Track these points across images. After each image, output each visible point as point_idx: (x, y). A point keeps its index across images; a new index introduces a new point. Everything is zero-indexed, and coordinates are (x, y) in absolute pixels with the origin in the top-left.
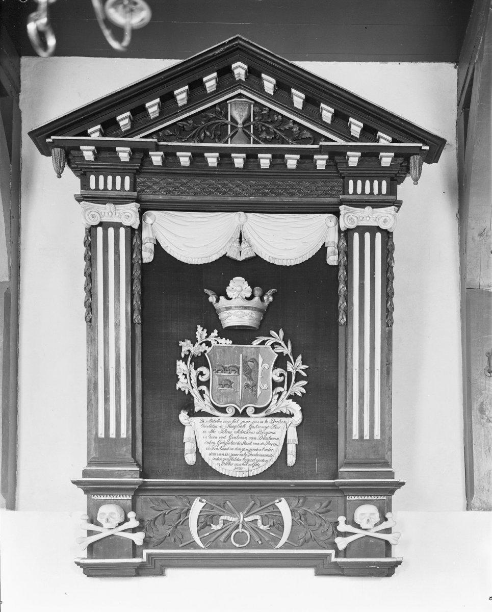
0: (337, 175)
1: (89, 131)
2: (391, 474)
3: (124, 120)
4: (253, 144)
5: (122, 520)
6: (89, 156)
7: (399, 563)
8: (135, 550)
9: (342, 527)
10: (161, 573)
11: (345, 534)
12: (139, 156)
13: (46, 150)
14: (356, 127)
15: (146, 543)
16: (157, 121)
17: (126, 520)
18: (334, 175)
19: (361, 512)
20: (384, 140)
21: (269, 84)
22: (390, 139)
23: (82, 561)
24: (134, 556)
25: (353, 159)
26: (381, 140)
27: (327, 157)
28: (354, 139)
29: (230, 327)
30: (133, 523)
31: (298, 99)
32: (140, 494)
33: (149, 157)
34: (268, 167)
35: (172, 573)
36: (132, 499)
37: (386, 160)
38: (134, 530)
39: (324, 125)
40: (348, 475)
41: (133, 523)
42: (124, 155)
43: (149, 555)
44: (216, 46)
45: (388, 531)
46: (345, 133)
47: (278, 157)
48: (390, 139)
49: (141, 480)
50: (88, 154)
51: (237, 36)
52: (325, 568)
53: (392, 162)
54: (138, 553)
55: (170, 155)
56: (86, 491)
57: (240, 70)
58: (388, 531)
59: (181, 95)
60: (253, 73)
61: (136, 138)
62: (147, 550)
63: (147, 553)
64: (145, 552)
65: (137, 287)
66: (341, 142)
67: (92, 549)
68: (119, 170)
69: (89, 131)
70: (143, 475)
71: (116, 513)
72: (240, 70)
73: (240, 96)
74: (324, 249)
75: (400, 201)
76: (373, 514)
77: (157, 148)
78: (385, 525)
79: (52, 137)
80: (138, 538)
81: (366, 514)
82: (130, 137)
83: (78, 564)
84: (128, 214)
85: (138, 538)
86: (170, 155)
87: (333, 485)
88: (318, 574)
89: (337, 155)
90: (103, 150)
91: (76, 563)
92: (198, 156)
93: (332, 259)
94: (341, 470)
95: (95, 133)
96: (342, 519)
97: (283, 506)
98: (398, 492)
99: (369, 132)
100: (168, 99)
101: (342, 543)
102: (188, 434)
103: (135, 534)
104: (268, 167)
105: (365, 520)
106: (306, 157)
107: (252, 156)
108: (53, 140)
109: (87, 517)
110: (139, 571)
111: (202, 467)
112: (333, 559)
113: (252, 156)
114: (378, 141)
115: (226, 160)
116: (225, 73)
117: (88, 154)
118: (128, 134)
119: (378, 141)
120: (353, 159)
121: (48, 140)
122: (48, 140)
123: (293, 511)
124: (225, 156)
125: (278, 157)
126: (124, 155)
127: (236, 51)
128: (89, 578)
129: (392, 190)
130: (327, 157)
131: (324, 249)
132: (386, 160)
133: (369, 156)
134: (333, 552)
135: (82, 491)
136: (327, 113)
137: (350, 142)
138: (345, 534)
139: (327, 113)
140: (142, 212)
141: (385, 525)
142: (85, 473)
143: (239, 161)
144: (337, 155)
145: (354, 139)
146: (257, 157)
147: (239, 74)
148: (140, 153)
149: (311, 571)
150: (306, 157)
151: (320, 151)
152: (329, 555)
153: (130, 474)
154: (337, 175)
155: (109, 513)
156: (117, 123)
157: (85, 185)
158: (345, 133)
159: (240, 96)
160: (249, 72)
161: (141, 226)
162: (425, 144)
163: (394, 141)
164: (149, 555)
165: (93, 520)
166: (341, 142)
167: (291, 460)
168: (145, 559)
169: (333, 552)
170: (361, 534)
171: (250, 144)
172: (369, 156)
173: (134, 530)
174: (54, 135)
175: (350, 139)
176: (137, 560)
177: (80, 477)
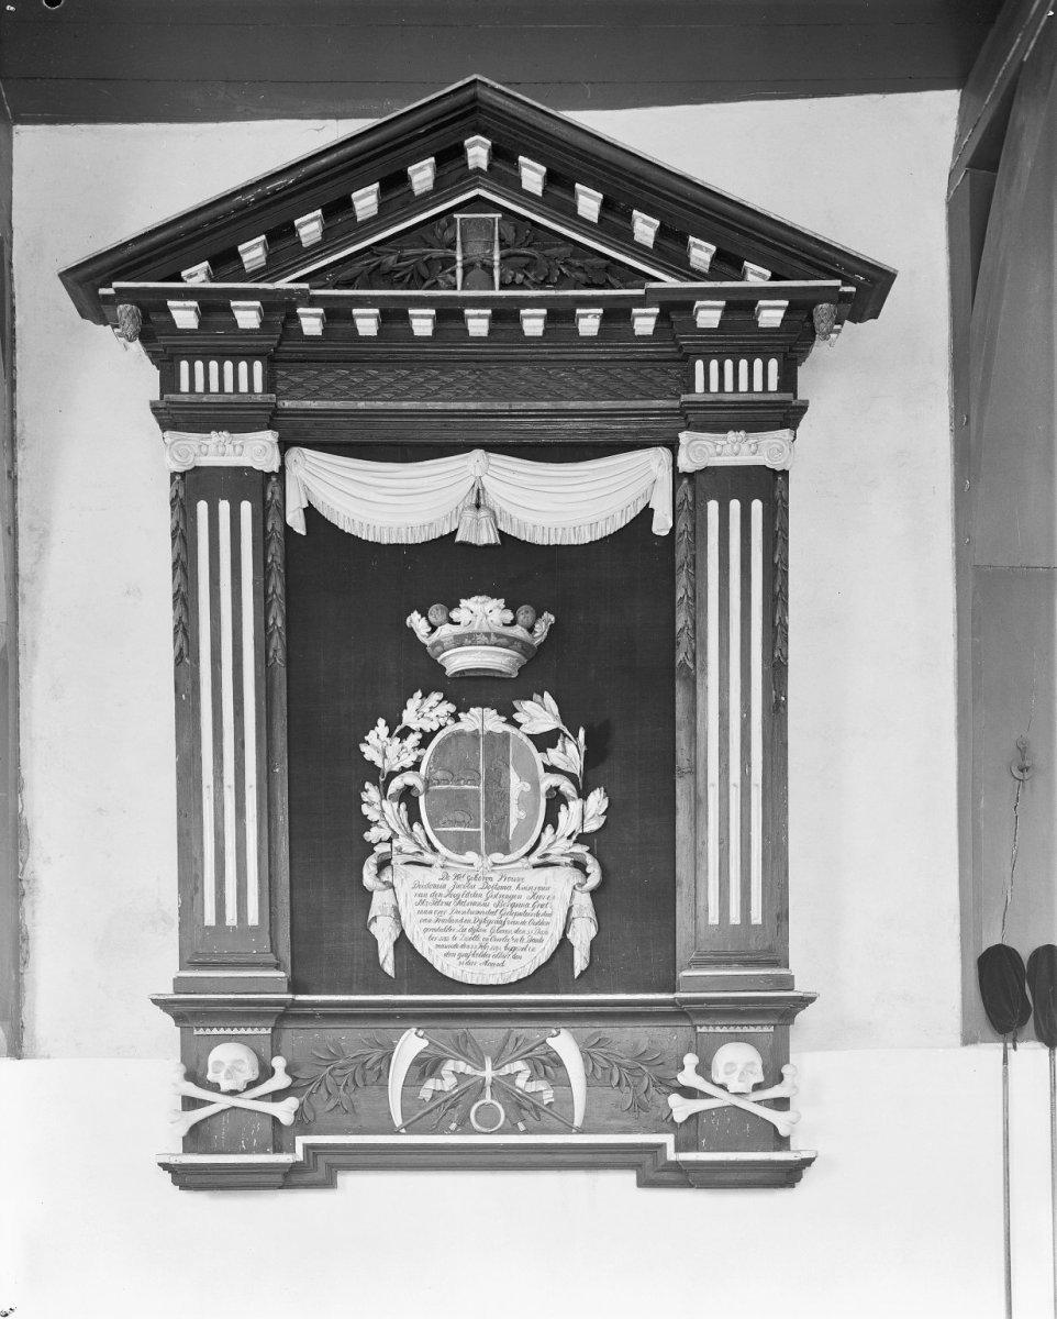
0: (674, 349)
1: (184, 274)
2: (787, 982)
3: (253, 253)
4: (501, 289)
5: (252, 1075)
6: (311, 326)
7: (808, 1162)
8: (278, 1137)
9: (688, 1077)
10: (329, 1183)
11: (689, 1093)
12: (279, 318)
13: (95, 308)
14: (701, 254)
15: (303, 1123)
16: (319, 249)
17: (267, 1072)
18: (670, 350)
19: (724, 1062)
20: (756, 276)
21: (532, 176)
22: (768, 274)
23: (172, 1161)
24: (278, 1149)
25: (709, 316)
26: (750, 277)
27: (657, 310)
28: (697, 275)
29: (463, 672)
30: (280, 1081)
31: (589, 203)
32: (285, 1026)
33: (296, 317)
34: (541, 334)
35: (352, 1183)
36: (272, 1035)
37: (771, 316)
38: (277, 1096)
39: (638, 250)
40: (696, 980)
41: (280, 1081)
42: (247, 317)
43: (307, 1147)
44: (433, 97)
45: (782, 1104)
46: (682, 268)
47: (561, 316)
48: (768, 274)
49: (290, 996)
50: (185, 316)
51: (475, 76)
52: (656, 1173)
53: (722, 317)
54: (285, 1143)
55: (337, 315)
56: (179, 1019)
57: (478, 152)
58: (782, 1104)
59: (366, 201)
60: (503, 155)
61: (282, 284)
62: (304, 1137)
63: (304, 1145)
64: (301, 1141)
65: (277, 585)
66: (670, 282)
67: (196, 1138)
68: (237, 348)
69: (184, 274)
70: (295, 986)
71: (246, 1061)
72: (478, 152)
73: (478, 203)
74: (647, 514)
75: (803, 401)
76: (753, 1063)
77: (313, 302)
78: (776, 1092)
79: (116, 284)
80: (285, 1111)
81: (737, 1063)
82: (270, 282)
83: (165, 1166)
84: (256, 450)
85: (285, 1111)
86: (337, 315)
87: (672, 1003)
88: (643, 1183)
89: (675, 310)
90: (213, 307)
91: (160, 1164)
92: (394, 316)
93: (661, 525)
94: (685, 973)
95: (197, 276)
96: (691, 1060)
97: (564, 1044)
98: (803, 1016)
99: (728, 262)
100: (337, 209)
101: (681, 1108)
102: (381, 902)
103: (275, 1104)
104: (541, 334)
105: (736, 1075)
106: (617, 315)
107: (505, 316)
108: (116, 289)
109: (182, 1069)
110: (288, 1178)
111: (415, 968)
112: (671, 1155)
113: (505, 316)
114: (742, 278)
115: (340, 326)
116: (450, 158)
117: (185, 316)
118: (257, 275)
119: (742, 278)
120: (709, 316)
121: (103, 291)
122: (103, 291)
123: (587, 1056)
124: (450, 315)
125: (561, 316)
126: (247, 317)
127: (469, 113)
128: (184, 1193)
129: (788, 381)
130: (656, 310)
131: (647, 514)
132: (771, 316)
133: (741, 306)
134: (668, 1139)
135: (169, 1020)
136: (645, 228)
137: (699, 281)
138: (689, 1093)
139: (645, 228)
140: (284, 446)
141: (776, 1092)
142: (179, 984)
143: (478, 325)
144: (675, 310)
145: (697, 275)
146: (685, 243)
147: (476, 156)
148: (279, 310)
149: (630, 1177)
150: (617, 315)
151: (641, 302)
152: (661, 1146)
153: (271, 983)
154: (674, 349)
155: (230, 1061)
156: (237, 257)
157: (169, 382)
158: (682, 268)
159: (478, 203)
160: (495, 153)
161: (283, 468)
162: (846, 282)
163: (774, 277)
164: (307, 1147)
165: (195, 1075)
166: (670, 282)
167: (580, 962)
168: (299, 1155)
169: (668, 1139)
170: (723, 1099)
171: (493, 289)
172: (741, 306)
173: (277, 1096)
174: (118, 277)
175: (686, 275)
176: (284, 1158)
177: (167, 991)
